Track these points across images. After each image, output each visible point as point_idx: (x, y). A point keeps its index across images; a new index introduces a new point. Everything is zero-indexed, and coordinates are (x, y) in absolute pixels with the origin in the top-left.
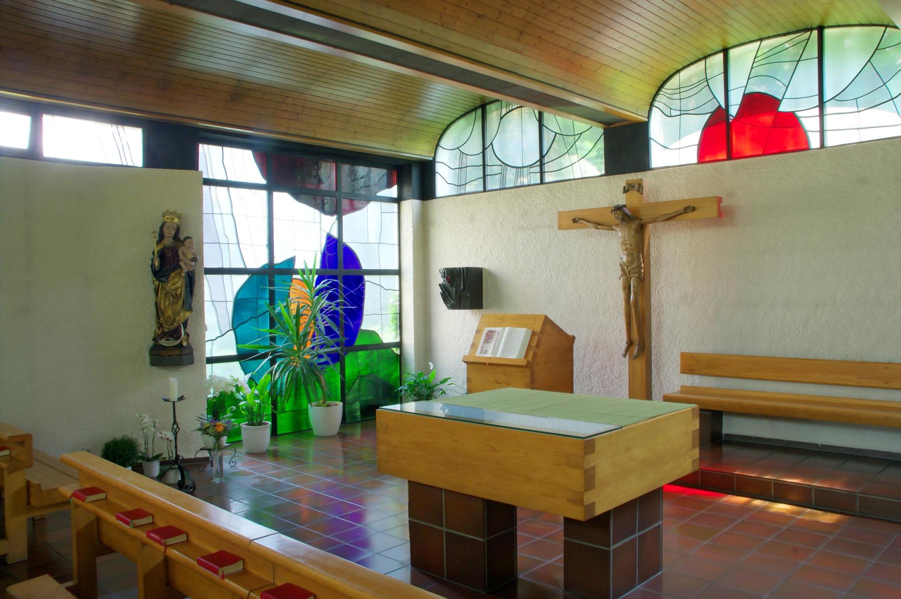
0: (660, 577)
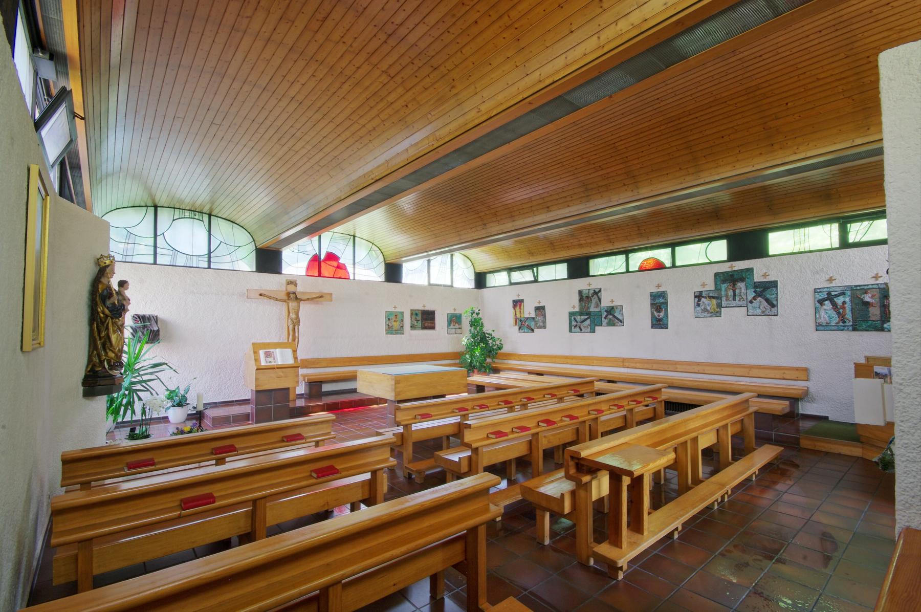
0: (575, 530)
